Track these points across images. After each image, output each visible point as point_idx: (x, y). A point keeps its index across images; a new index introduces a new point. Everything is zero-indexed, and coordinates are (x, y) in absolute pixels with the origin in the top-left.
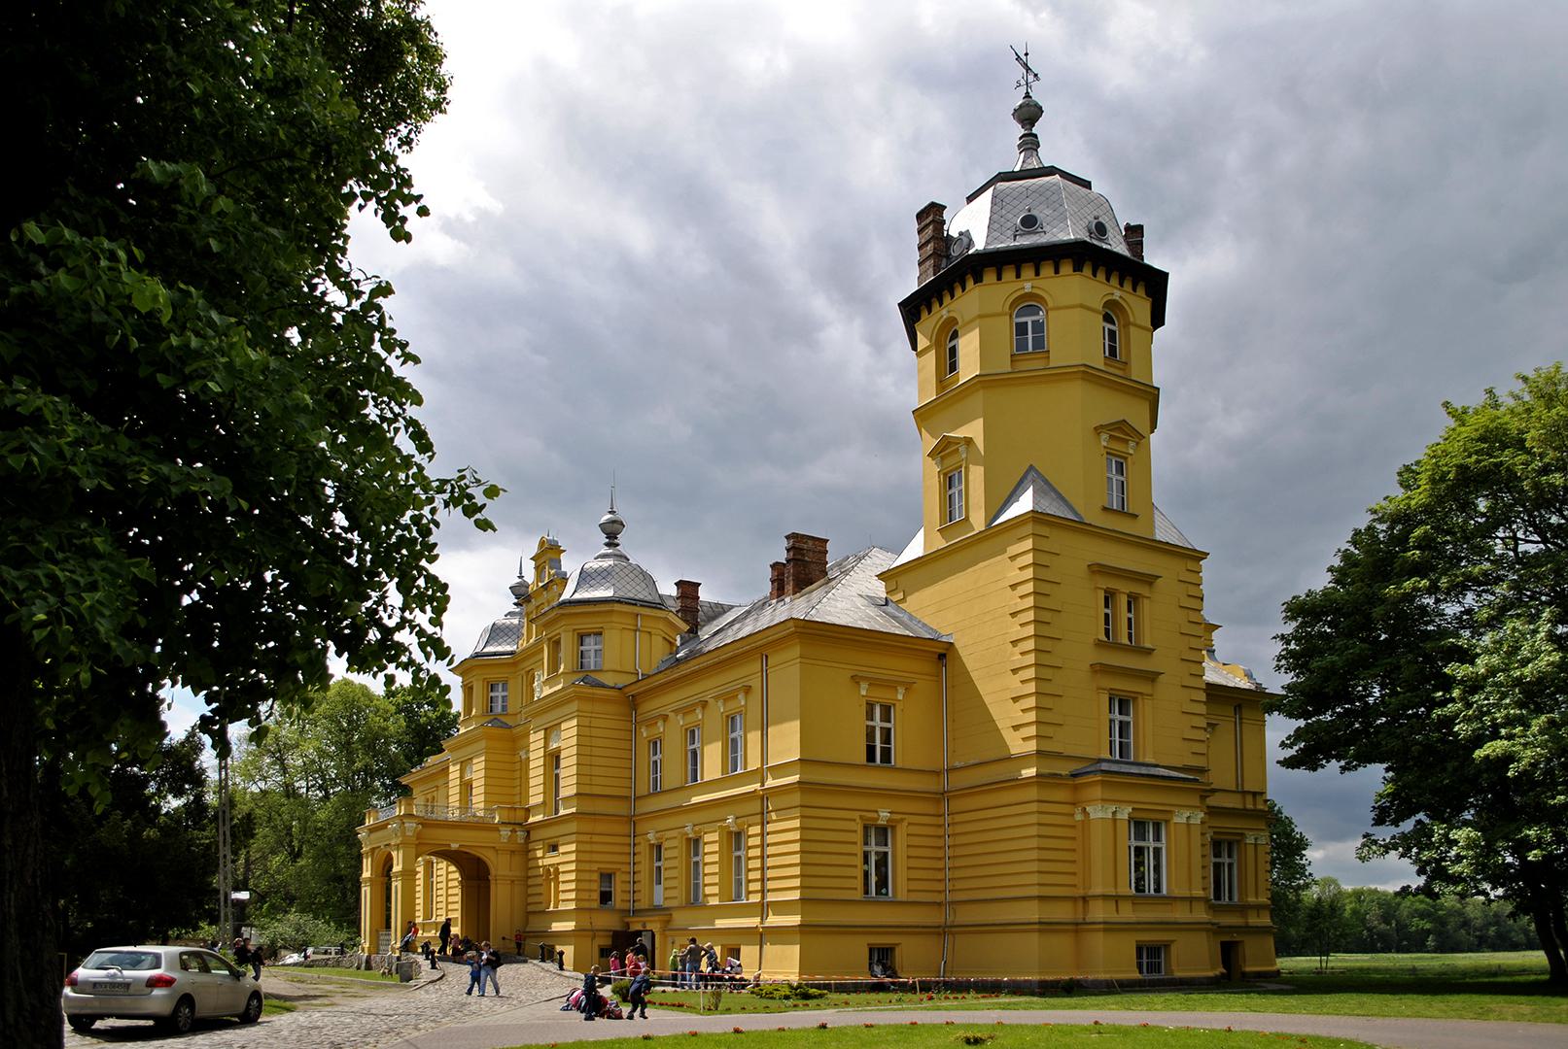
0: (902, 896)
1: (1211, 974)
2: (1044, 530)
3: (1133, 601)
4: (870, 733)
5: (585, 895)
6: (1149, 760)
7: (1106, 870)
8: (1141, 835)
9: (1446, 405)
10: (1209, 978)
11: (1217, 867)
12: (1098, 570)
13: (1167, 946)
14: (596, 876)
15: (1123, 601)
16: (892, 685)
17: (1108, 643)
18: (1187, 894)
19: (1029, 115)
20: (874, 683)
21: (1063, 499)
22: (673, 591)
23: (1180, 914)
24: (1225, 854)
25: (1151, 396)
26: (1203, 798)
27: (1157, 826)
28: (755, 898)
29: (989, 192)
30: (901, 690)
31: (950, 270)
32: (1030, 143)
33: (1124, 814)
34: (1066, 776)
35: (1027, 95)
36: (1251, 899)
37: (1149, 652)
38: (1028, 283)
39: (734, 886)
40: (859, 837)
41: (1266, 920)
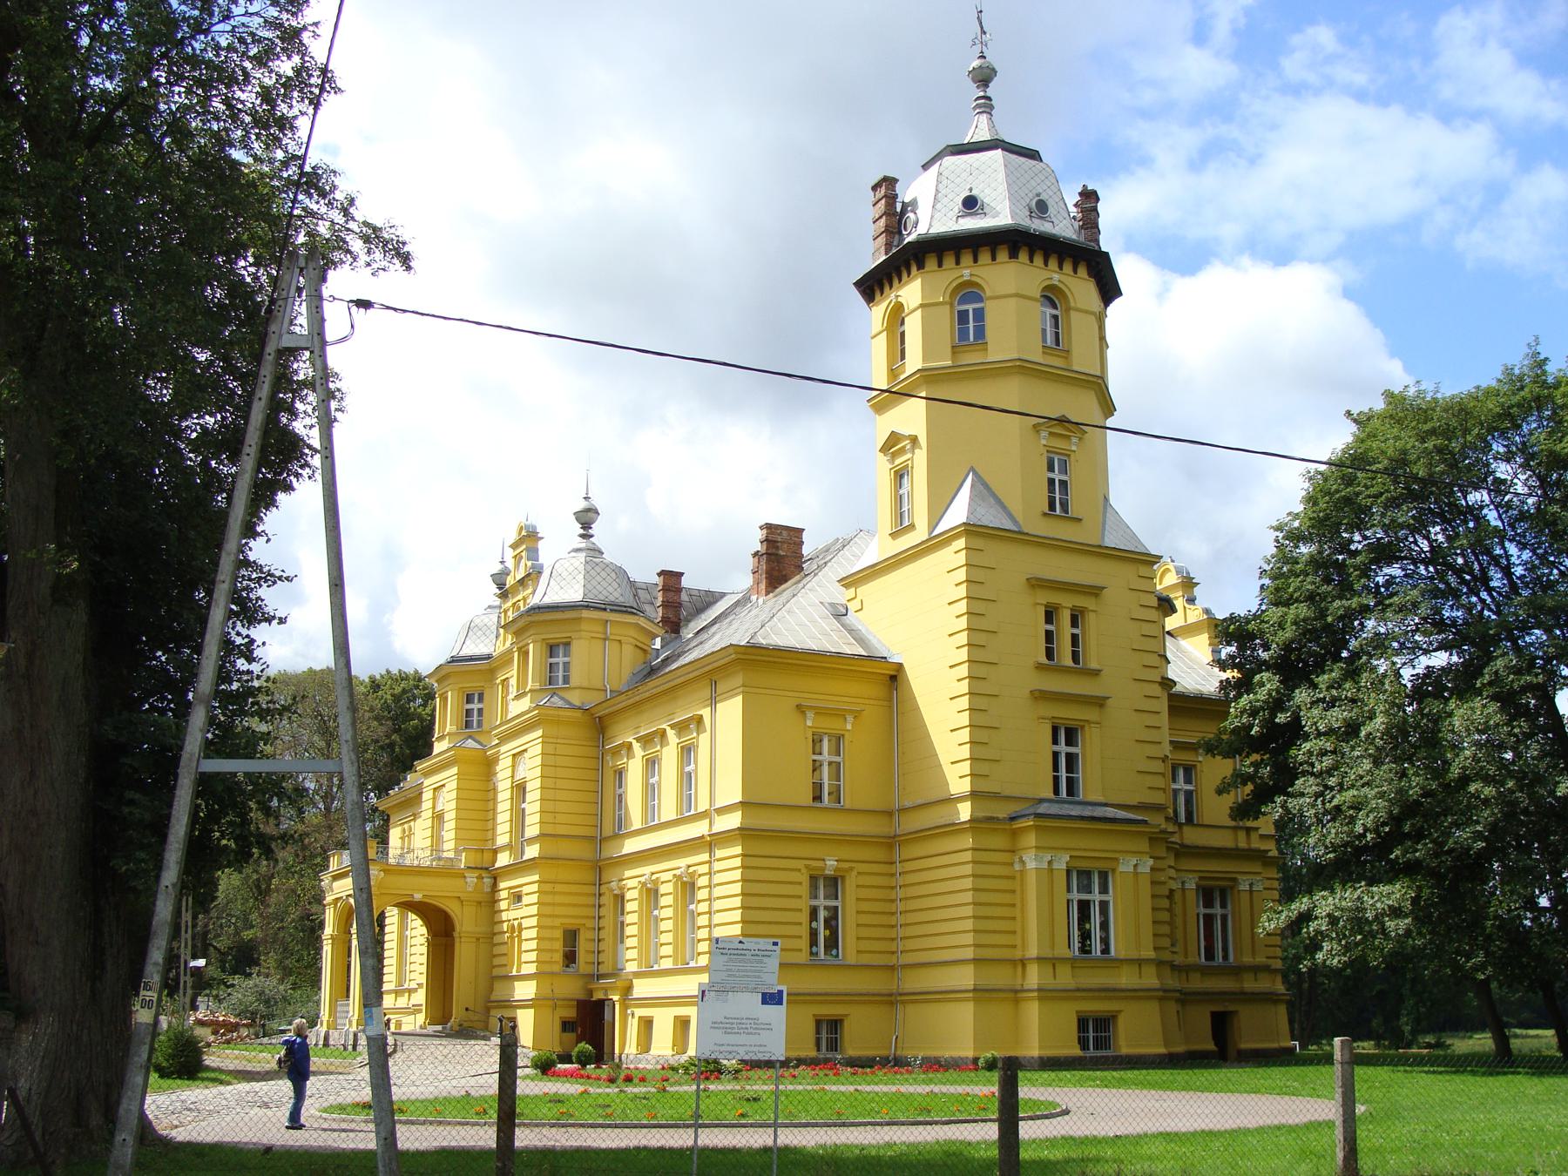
0: (851, 960)
2: (979, 543)
6: (1092, 798)
7: (1039, 925)
9: (1349, 413)
10: (1160, 1056)
12: (1037, 584)
14: (559, 934)
15: (1065, 617)
16: (841, 714)
18: (1134, 955)
20: (820, 712)
21: (1004, 507)
23: (1126, 978)
24: (1218, 903)
25: (1097, 385)
27: (1104, 876)
30: (850, 719)
33: (1061, 865)
36: (1247, 960)
37: (1096, 673)
38: (966, 271)
40: (804, 890)
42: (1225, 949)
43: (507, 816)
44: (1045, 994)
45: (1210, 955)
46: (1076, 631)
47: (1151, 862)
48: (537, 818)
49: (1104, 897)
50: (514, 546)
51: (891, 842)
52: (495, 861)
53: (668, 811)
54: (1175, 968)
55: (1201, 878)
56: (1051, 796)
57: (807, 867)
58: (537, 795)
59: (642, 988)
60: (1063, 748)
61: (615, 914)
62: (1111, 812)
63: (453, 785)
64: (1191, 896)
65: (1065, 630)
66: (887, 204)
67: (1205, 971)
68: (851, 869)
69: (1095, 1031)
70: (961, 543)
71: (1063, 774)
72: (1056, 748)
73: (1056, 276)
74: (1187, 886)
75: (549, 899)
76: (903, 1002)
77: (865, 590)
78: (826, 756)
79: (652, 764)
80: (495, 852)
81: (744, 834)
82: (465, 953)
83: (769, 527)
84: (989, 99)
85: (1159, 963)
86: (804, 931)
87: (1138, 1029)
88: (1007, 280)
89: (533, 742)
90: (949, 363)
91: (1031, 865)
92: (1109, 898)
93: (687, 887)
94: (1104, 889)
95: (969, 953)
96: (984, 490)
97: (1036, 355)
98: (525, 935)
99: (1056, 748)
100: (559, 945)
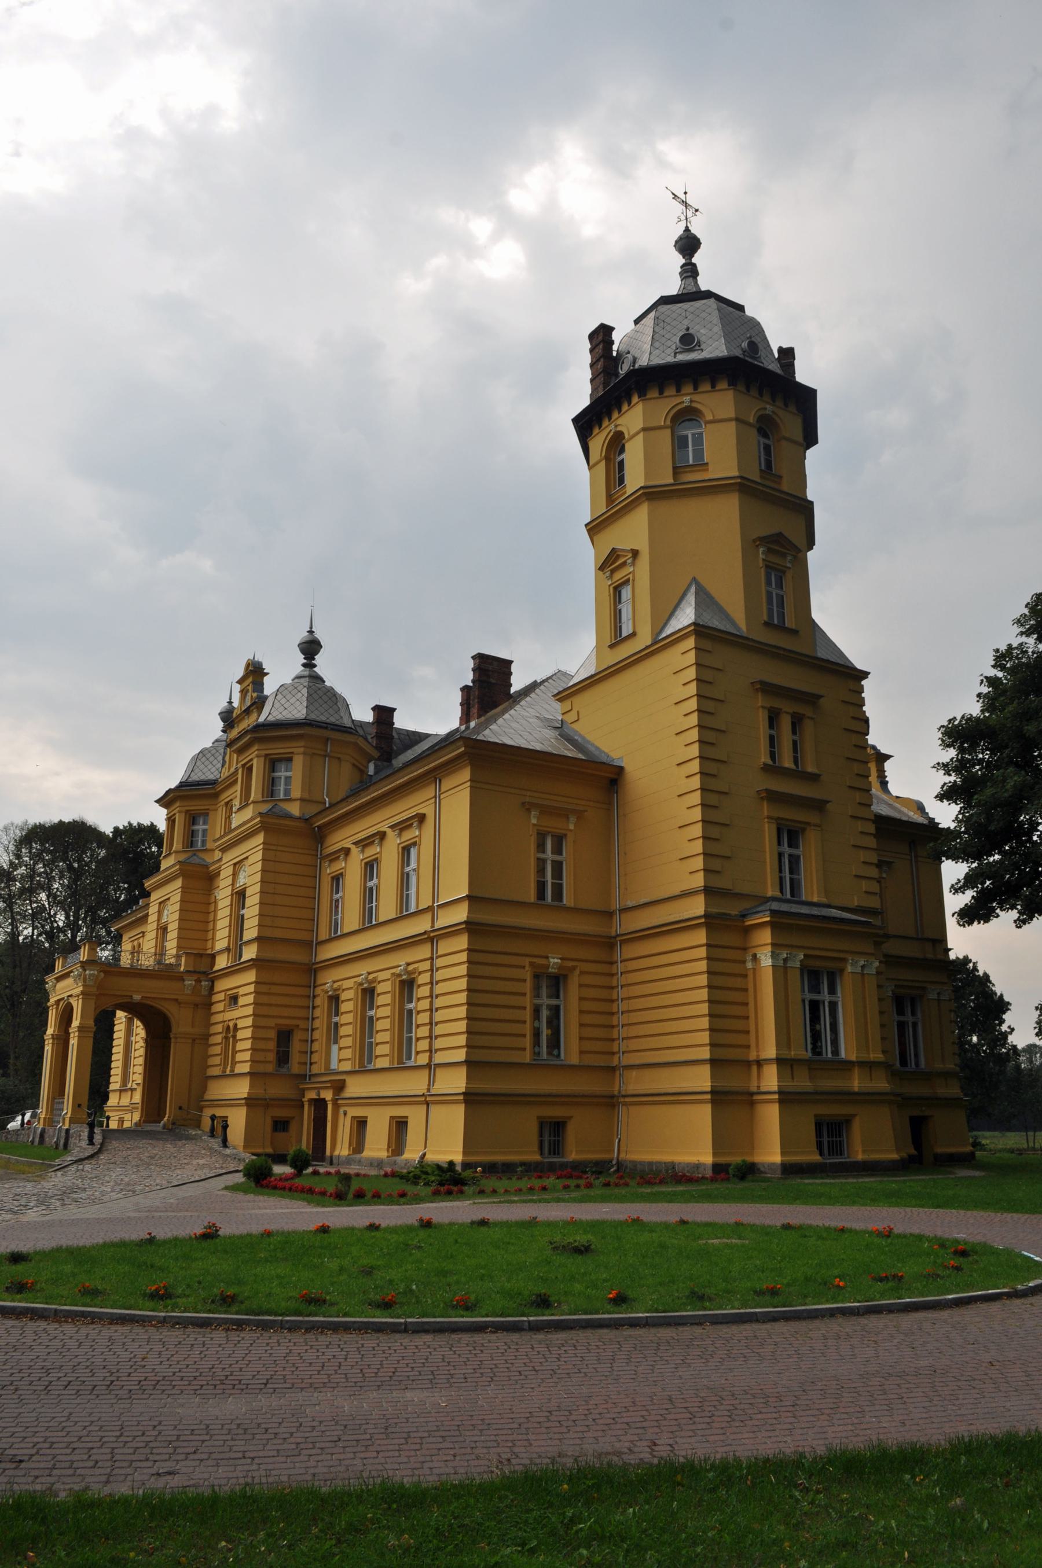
0: (574, 1060)
1: (895, 1156)
2: (707, 645)
4: (541, 864)
5: (260, 1057)
8: (815, 988)
11: (902, 1026)
12: (766, 688)
13: (848, 1121)
14: (272, 1034)
15: (786, 723)
16: (563, 814)
17: (772, 769)
19: (688, 244)
20: (546, 811)
22: (368, 717)
23: (856, 1083)
25: (806, 509)
26: (878, 944)
28: (423, 1059)
29: (652, 315)
31: (617, 382)
32: (690, 271)
36: (939, 1066)
39: (403, 1046)
41: (954, 1090)
42: (916, 1055)
43: (226, 922)
48: (255, 921)
50: (239, 682)
51: (610, 943)
52: (213, 964)
53: (387, 908)
56: (778, 894)
58: (256, 899)
59: (355, 1087)
61: (329, 1017)
63: (177, 897)
66: (604, 349)
68: (574, 968)
70: (690, 643)
75: (265, 999)
78: (549, 854)
79: (370, 867)
80: (213, 957)
81: (471, 927)
82: (178, 1054)
84: (694, 265)
87: (872, 1138)
89: (254, 850)
90: (671, 481)
93: (407, 985)
96: (705, 600)
98: (240, 1035)
100: (272, 1045)
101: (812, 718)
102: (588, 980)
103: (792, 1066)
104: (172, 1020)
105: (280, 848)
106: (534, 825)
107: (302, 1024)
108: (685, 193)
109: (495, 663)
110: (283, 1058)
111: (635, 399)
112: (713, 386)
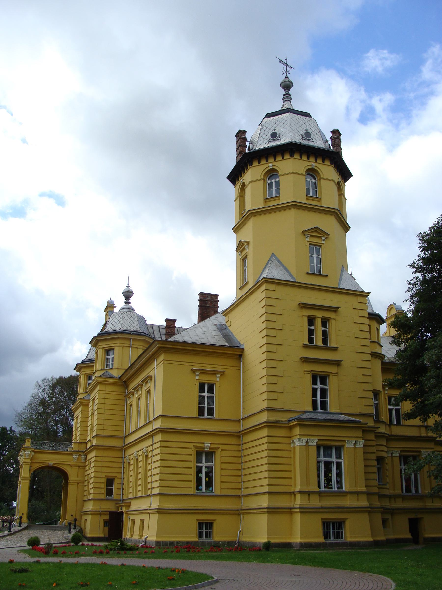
0: (218, 493)
2: (272, 287)
3: (325, 323)
6: (333, 411)
12: (303, 306)
14: (104, 480)
15: (319, 322)
16: (213, 373)
18: (354, 489)
19: (287, 86)
20: (203, 372)
23: (348, 502)
30: (218, 375)
32: (287, 97)
33: (313, 444)
34: (280, 424)
35: (286, 77)
37: (335, 349)
40: (193, 458)
42: (416, 487)
44: (304, 510)
45: (408, 489)
46: (325, 329)
47: (363, 442)
49: (339, 460)
54: (381, 496)
55: (401, 451)
57: (194, 446)
60: (318, 386)
62: (342, 417)
64: (397, 461)
65: (318, 328)
67: (404, 498)
68: (218, 448)
69: (334, 529)
71: (319, 399)
72: (314, 386)
73: (313, 164)
74: (394, 455)
76: (244, 514)
77: (232, 315)
83: (201, 294)
84: (290, 95)
85: (368, 494)
86: (193, 478)
88: (287, 165)
91: (297, 444)
92: (342, 460)
94: (339, 456)
95: (266, 489)
97: (303, 199)
99: (314, 386)
100: (104, 486)
101: (335, 319)
102: (224, 453)
103: (309, 495)
104: (69, 476)
105: (106, 392)
106: (197, 379)
107: (118, 476)
108: (286, 59)
109: (209, 297)
110: (109, 492)
111: (249, 167)
112: (283, 157)
